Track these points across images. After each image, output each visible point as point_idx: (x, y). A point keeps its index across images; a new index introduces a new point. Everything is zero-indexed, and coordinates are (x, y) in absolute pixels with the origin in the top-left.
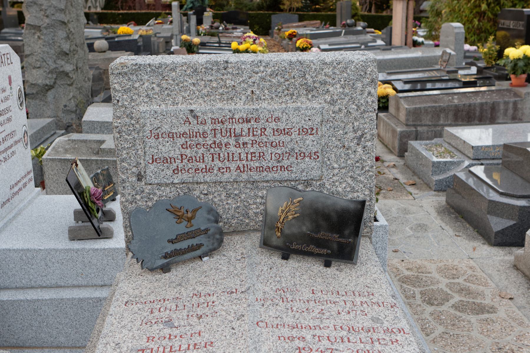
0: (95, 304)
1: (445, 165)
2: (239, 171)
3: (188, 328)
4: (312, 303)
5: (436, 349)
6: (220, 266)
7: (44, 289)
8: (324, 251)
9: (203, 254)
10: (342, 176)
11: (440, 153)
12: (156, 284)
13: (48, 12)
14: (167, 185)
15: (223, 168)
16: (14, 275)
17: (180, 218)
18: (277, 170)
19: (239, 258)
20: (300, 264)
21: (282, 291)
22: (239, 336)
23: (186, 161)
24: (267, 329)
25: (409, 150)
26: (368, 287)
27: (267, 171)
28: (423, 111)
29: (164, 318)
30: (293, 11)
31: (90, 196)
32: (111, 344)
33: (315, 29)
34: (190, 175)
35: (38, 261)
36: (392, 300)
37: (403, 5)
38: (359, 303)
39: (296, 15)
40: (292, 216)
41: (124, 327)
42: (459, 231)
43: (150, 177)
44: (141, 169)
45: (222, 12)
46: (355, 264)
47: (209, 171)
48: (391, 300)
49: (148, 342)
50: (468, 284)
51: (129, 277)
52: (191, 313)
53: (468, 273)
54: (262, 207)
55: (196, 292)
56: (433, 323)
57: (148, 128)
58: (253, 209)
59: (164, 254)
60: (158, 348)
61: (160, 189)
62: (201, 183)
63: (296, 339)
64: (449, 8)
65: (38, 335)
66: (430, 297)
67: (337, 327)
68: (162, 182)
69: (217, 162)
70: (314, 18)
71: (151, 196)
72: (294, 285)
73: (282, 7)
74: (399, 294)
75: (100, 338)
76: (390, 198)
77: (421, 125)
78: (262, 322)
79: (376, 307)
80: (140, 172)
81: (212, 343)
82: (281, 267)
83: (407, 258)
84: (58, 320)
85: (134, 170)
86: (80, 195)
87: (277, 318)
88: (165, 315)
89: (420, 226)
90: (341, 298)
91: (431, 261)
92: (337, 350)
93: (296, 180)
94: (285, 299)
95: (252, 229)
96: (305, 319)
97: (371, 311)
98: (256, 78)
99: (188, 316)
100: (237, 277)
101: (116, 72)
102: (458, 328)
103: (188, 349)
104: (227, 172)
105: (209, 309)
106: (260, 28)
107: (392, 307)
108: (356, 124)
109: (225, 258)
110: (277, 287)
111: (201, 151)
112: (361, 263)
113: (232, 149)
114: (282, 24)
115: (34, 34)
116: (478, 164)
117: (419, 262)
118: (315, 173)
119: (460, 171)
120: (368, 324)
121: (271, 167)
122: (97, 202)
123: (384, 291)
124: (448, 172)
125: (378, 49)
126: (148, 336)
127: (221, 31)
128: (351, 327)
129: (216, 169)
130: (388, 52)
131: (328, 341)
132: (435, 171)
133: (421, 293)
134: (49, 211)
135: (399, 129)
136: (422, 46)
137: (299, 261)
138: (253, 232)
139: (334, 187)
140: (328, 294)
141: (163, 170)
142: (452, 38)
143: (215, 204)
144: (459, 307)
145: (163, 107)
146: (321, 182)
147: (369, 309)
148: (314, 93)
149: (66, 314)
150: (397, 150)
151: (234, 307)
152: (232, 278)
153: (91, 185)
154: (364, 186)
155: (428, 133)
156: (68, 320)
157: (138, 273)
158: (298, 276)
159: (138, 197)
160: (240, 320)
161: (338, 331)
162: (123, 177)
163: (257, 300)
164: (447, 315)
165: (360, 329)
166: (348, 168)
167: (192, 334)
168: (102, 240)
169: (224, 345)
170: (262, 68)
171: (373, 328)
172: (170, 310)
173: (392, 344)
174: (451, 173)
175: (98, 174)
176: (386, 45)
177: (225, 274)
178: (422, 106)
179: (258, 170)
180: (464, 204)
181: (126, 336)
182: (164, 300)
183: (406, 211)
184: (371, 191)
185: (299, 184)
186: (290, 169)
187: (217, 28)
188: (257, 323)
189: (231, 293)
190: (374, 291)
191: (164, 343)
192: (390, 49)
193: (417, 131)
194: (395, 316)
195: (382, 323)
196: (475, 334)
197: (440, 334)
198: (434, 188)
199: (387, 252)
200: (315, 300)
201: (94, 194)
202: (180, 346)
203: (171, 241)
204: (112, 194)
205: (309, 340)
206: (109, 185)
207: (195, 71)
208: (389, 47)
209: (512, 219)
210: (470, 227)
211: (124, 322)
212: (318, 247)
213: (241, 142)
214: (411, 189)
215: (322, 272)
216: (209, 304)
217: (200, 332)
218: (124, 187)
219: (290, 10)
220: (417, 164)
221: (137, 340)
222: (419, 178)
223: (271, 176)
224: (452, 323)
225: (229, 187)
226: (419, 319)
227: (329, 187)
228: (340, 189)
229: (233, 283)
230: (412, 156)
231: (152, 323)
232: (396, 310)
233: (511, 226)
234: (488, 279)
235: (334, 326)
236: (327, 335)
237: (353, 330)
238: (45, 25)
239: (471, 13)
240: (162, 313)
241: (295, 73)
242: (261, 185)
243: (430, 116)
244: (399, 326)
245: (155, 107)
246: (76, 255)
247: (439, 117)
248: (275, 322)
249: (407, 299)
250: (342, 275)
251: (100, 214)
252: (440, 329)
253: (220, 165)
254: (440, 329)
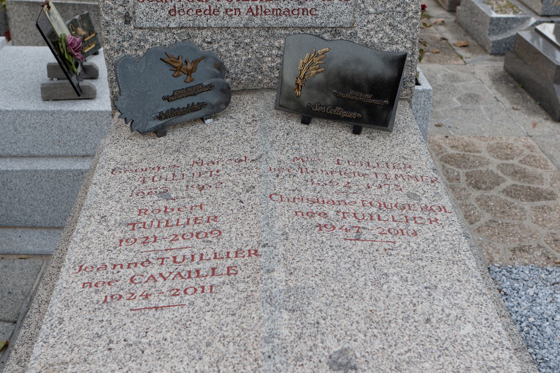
0: (75, 178)
1: (506, 23)
2: (251, 14)
3: (187, 200)
4: (336, 176)
5: (481, 239)
6: (227, 130)
7: (15, 159)
8: (354, 115)
9: (206, 115)
10: (379, 24)
11: (501, 7)
12: (148, 150)
14: (161, 30)
15: (231, 10)
17: (177, 70)
18: (298, 14)
19: (250, 120)
20: (324, 130)
21: (300, 160)
22: (249, 210)
24: (282, 203)
26: (405, 158)
27: (286, 15)
29: (159, 189)
31: (67, 46)
32: (96, 217)
34: (191, 18)
35: (5, 125)
36: (433, 173)
38: (393, 176)
40: (315, 71)
41: (110, 198)
42: (518, 104)
43: (141, 19)
44: (129, 9)
46: (391, 131)
47: (214, 13)
48: (431, 174)
49: (139, 215)
50: (524, 166)
51: (116, 141)
52: (191, 183)
53: (525, 153)
54: (279, 61)
55: (197, 159)
56: (478, 209)
59: (158, 114)
60: (152, 222)
61: (153, 35)
62: (204, 28)
63: (316, 215)
65: (9, 212)
66: (478, 179)
67: (366, 202)
68: (155, 25)
71: (142, 44)
72: (316, 154)
74: (440, 169)
75: (83, 210)
76: (435, 62)
78: (276, 194)
79: (413, 181)
80: (128, 12)
81: (216, 217)
82: (300, 133)
83: (452, 133)
84: (33, 195)
85: (120, 9)
86: (54, 45)
87: (294, 190)
88: (160, 185)
89: (470, 96)
90: (372, 170)
91: (481, 138)
92: (364, 228)
93: (322, 28)
94: (304, 170)
95: (265, 87)
96: (327, 193)
97: (407, 186)
99: (187, 186)
100: (246, 143)
102: (509, 216)
103: (188, 223)
104: (235, 14)
105: (213, 179)
107: (432, 182)
109: (232, 120)
110: (294, 155)
112: (397, 131)
116: (548, 22)
117: (466, 138)
118: (346, 19)
119: (525, 30)
120: (403, 200)
121: (291, 9)
122: (76, 54)
123: (424, 163)
124: (509, 31)
126: (140, 208)
128: (382, 203)
129: (222, 10)
131: (354, 219)
132: (493, 30)
133: (467, 175)
134: (17, 65)
137: (322, 127)
138: (268, 91)
139: (368, 37)
140: (357, 164)
141: (157, 11)
143: (221, 55)
144: (511, 192)
146: (353, 31)
147: (405, 184)
149: (42, 189)
151: (242, 177)
152: (241, 144)
153: (67, 33)
154: (406, 37)
156: (44, 196)
157: (127, 136)
158: (320, 143)
159: (126, 44)
160: (250, 192)
161: (367, 208)
162: (107, 18)
163: (271, 170)
164: (497, 201)
165: (393, 205)
166: (386, 14)
167: (192, 207)
168: (82, 101)
169: (230, 220)
171: (409, 205)
172: (166, 180)
173: (431, 223)
174: (513, 33)
175: (75, 20)
177: (233, 139)
179: (275, 13)
180: (527, 71)
181: (113, 208)
182: (159, 168)
183: (454, 78)
184: (414, 43)
185: (325, 32)
186: (314, 13)
188: (270, 196)
189: (239, 161)
190: (412, 163)
191: (158, 216)
194: (435, 193)
195: (420, 200)
196: (527, 223)
197: (486, 223)
198: (490, 51)
199: (429, 123)
200: (340, 172)
201: (71, 44)
202: (178, 220)
203: (167, 99)
204: (93, 46)
205: (332, 217)
206: (90, 35)
210: (532, 99)
211: (110, 193)
212: (345, 110)
214: (461, 52)
215: (350, 139)
216: (213, 173)
217: (201, 205)
218: (108, 32)
220: (471, 21)
221: (126, 213)
222: (473, 39)
223: (289, 21)
224: (501, 210)
225: (238, 34)
226: (463, 205)
227: (362, 38)
228: (376, 40)
229: (242, 150)
230: (465, 11)
231: (144, 193)
232: (437, 185)
234: (549, 161)
235: (363, 201)
236: (354, 212)
237: (385, 206)
240: (156, 183)
242: (278, 32)
244: (440, 203)
246: (51, 118)
248: (292, 196)
249: (450, 182)
250: (375, 143)
251: (79, 70)
252: (487, 217)
254: (487, 217)
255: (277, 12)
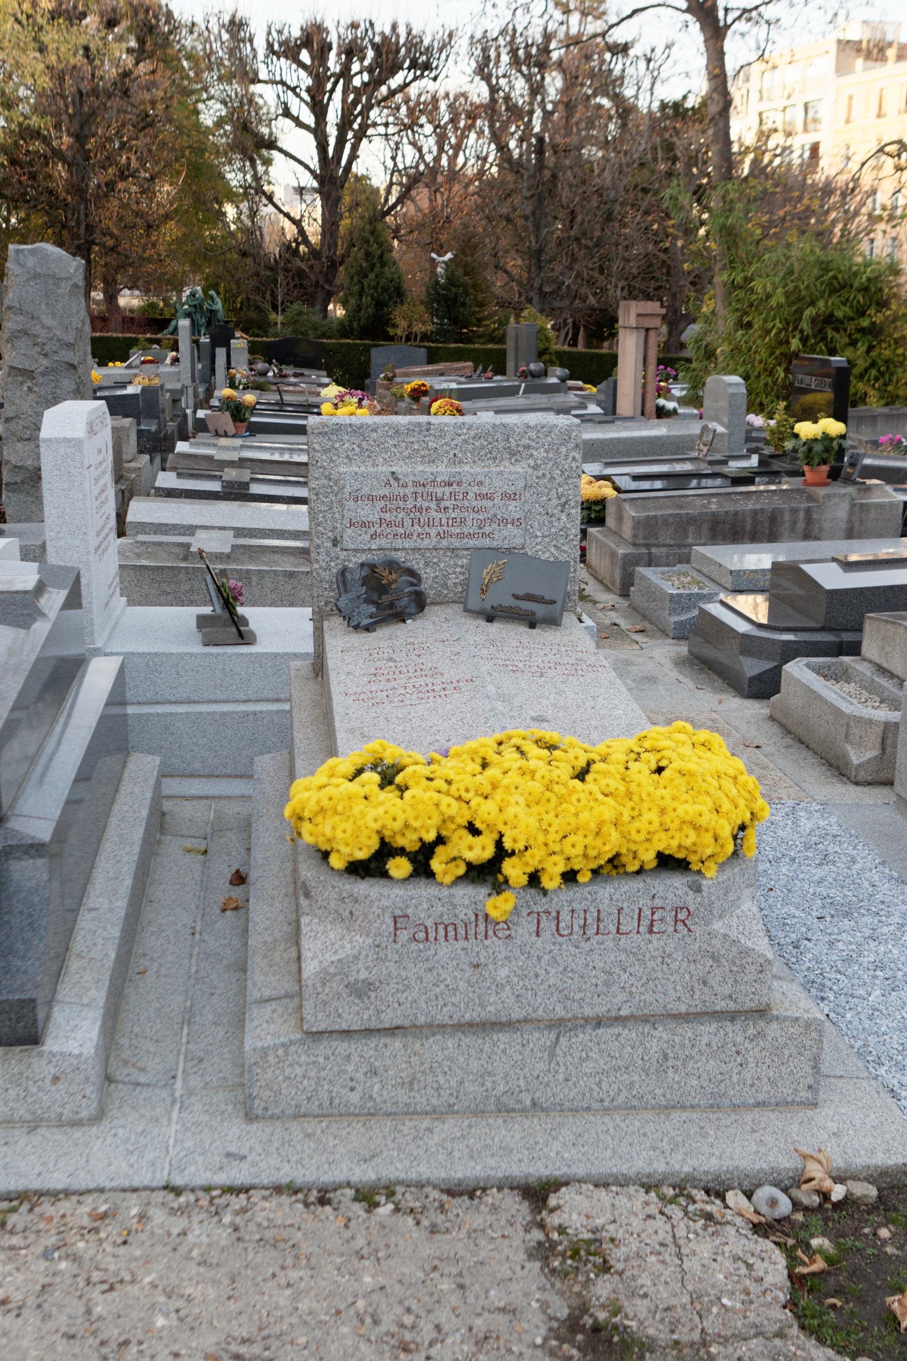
13: (47, 348)
14: (363, 551)
16: (137, 686)
23: (384, 525)
25: (637, 581)
28: (660, 522)
30: (415, 340)
33: (463, 379)
37: (637, 339)
39: (422, 350)
45: (265, 339)
57: (347, 490)
58: (452, 580)
64: (730, 344)
69: (416, 527)
70: (459, 356)
73: (391, 331)
77: (658, 546)
85: (330, 534)
98: (458, 440)
101: (316, 431)
106: (344, 373)
108: (560, 490)
111: (400, 516)
113: (433, 513)
114: (394, 367)
115: (22, 383)
118: (518, 542)
125: (590, 421)
127: (272, 380)
129: (415, 535)
130: (607, 426)
132: (675, 609)
135: (621, 551)
136: (677, 417)
142: (724, 403)
145: (363, 468)
148: (518, 457)
150: (618, 585)
155: (667, 558)
159: (333, 564)
170: (465, 431)
176: (605, 414)
178: (660, 513)
187: (264, 374)
192: (612, 422)
193: (650, 554)
198: (671, 635)
207: (397, 432)
208: (609, 418)
209: (773, 660)
213: (442, 506)
219: (408, 339)
223: (471, 543)
233: (770, 670)
238: (42, 368)
239: (771, 354)
241: (499, 436)
242: (461, 553)
243: (672, 530)
245: (356, 469)
247: (685, 531)
253: (420, 530)
255: (461, 536)
